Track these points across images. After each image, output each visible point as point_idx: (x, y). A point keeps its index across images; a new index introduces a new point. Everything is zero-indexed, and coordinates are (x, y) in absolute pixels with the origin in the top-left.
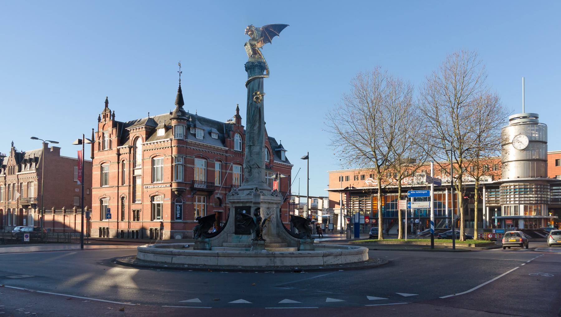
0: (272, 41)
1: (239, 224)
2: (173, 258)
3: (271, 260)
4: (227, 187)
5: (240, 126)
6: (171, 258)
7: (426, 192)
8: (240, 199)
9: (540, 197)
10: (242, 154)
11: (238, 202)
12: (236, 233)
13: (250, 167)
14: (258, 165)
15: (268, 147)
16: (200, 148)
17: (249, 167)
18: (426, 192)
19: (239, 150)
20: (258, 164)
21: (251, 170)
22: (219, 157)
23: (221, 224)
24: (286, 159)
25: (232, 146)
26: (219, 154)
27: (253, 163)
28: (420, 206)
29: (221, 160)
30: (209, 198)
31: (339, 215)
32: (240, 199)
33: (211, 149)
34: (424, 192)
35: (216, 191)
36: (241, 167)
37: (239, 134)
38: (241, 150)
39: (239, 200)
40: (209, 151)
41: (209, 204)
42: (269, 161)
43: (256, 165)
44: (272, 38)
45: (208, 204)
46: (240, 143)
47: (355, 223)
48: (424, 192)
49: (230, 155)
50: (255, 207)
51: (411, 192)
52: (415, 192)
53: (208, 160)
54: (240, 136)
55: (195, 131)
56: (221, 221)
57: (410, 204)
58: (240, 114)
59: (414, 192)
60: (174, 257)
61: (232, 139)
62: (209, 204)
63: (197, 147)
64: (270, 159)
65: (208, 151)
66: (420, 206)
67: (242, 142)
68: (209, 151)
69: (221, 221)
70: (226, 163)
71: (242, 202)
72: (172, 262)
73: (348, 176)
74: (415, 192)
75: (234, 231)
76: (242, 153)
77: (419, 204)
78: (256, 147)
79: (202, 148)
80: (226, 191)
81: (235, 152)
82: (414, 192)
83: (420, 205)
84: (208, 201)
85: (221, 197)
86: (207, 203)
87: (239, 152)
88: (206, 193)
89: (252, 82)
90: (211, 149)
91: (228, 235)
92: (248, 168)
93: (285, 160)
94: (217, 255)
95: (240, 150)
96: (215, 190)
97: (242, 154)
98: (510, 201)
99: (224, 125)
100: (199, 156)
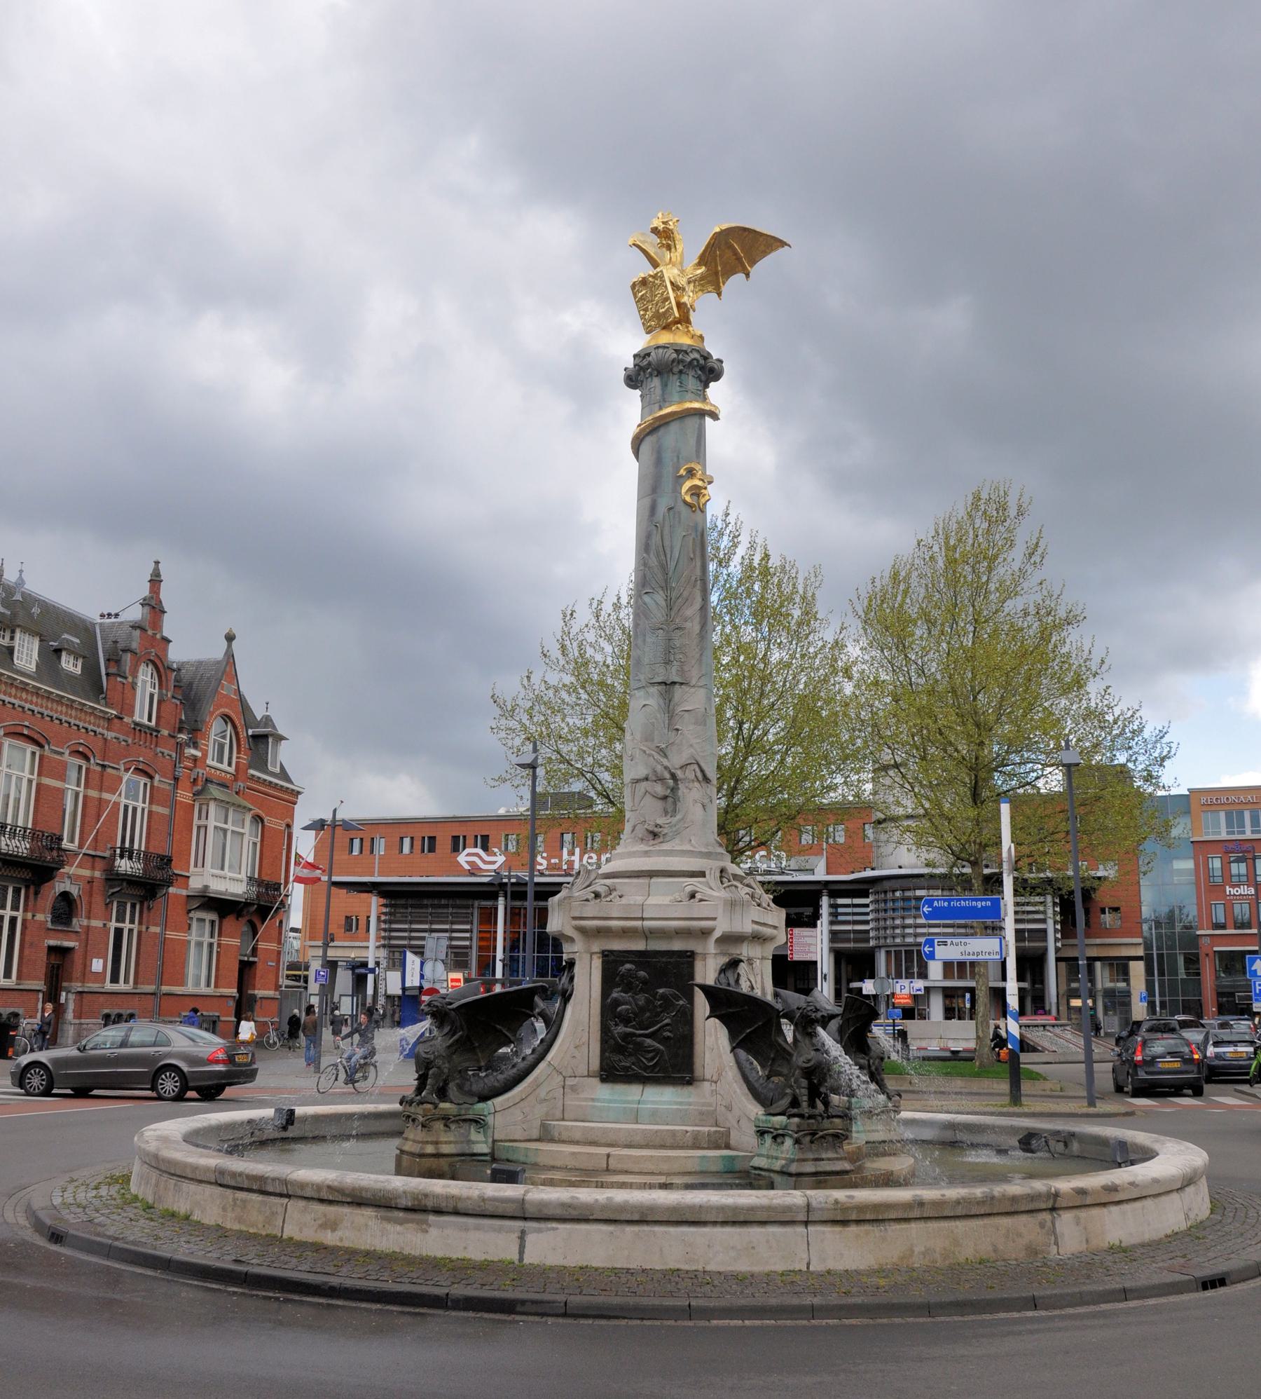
0: (753, 271)
1: (629, 1030)
2: (530, 1239)
3: (1042, 1225)
4: (99, 853)
5: (158, 636)
6: (514, 1237)
7: (989, 903)
8: (643, 919)
9: (909, 926)
10: (156, 736)
11: (625, 933)
12: (609, 1074)
13: (673, 776)
14: (702, 771)
15: (237, 722)
16: (26, 701)
17: (667, 775)
18: (989, 903)
19: (145, 721)
20: (702, 764)
21: (674, 790)
22: (82, 741)
23: (64, 994)
24: (282, 767)
25: (127, 707)
26: (83, 730)
27: (684, 758)
28: (969, 954)
29: (90, 754)
30: (36, 893)
31: (340, 963)
32: (643, 919)
33: (59, 709)
34: (979, 904)
35: (66, 870)
36: (145, 785)
37: (150, 667)
38: (153, 723)
39: (638, 923)
40: (52, 717)
41: (33, 916)
42: (232, 770)
43: (696, 767)
44: (753, 262)
45: (29, 915)
46: (152, 696)
47: (404, 989)
48: (979, 904)
49: (118, 735)
50: (724, 954)
51: (936, 904)
52: (949, 904)
53: (46, 747)
54: (155, 674)
55: (12, 638)
56: (65, 984)
57: (932, 946)
58: (162, 596)
59: (946, 904)
60: (539, 1231)
61: (130, 679)
62: (33, 916)
63: (15, 697)
64: (237, 763)
65: (51, 714)
66: (974, 954)
67: (160, 694)
68: (52, 717)
69: (65, 984)
70: (103, 766)
71: (648, 934)
72: (527, 1261)
73: (430, 838)
74: (949, 904)
75: (595, 1064)
76: (155, 734)
77: (965, 944)
78: (693, 690)
79: (31, 703)
80: (93, 868)
81: (134, 729)
82: (946, 904)
83: (969, 949)
84: (31, 903)
85: (74, 891)
86: (25, 910)
87: (149, 728)
88: (27, 875)
89: (674, 427)
90: (59, 709)
91: (569, 1082)
92: (661, 779)
93: (278, 770)
94: (802, 1217)
95: (150, 720)
96: (61, 864)
97: (156, 736)
98: (904, 937)
99: (98, 631)
100: (18, 730)
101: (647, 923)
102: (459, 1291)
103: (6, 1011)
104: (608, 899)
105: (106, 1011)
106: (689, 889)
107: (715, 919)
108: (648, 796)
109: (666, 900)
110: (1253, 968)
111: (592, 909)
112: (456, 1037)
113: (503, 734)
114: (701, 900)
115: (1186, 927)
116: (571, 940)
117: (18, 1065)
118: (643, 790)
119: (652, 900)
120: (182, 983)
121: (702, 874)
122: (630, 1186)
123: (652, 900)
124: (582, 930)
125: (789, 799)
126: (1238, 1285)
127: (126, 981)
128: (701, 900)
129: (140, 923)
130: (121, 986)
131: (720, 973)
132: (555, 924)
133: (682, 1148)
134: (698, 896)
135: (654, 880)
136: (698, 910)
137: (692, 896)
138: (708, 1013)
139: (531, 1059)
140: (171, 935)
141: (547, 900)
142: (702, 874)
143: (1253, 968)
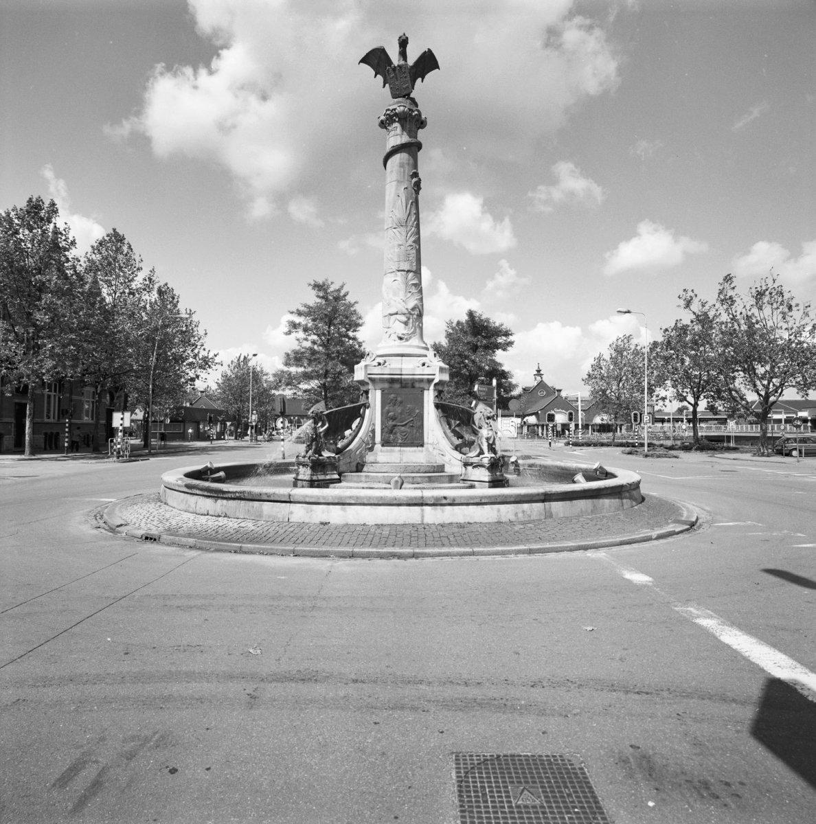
8: (401, 375)
32: (401, 375)
101: (403, 377)
102: (472, 502)
103: (2, 432)
105: (44, 431)
106: (422, 362)
108: (397, 321)
109: (411, 366)
111: (377, 370)
118: (394, 319)
120: (80, 418)
125: (130, 356)
126: (624, 546)
127: (54, 418)
129: (60, 392)
130: (52, 420)
133: (430, 473)
135: (404, 358)
136: (426, 371)
137: (424, 365)
139: (350, 438)
140: (74, 397)
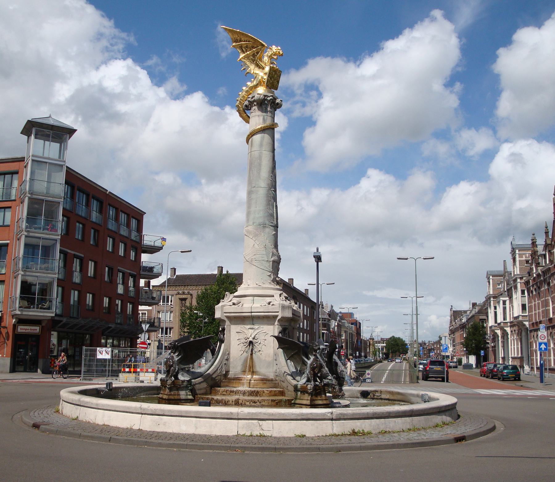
8: (252, 312)
104: (238, 305)
107: (278, 312)
109: (258, 305)
110: (541, 347)
112: (180, 357)
113: (256, 186)
114: (273, 305)
115: (470, 335)
116: (224, 321)
117: (128, 36)
119: (255, 305)
121: (273, 296)
122: (510, 311)
123: (255, 305)
124: (227, 317)
128: (273, 305)
131: (279, 333)
132: (218, 315)
134: (271, 304)
137: (269, 303)
138: (278, 347)
141: (462, 35)
142: (273, 296)
143: (541, 347)
